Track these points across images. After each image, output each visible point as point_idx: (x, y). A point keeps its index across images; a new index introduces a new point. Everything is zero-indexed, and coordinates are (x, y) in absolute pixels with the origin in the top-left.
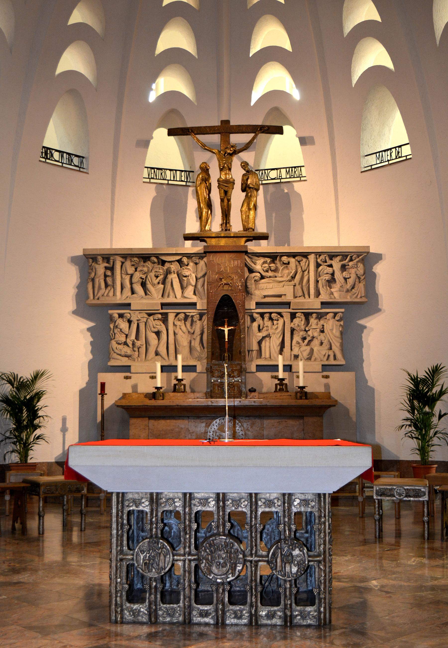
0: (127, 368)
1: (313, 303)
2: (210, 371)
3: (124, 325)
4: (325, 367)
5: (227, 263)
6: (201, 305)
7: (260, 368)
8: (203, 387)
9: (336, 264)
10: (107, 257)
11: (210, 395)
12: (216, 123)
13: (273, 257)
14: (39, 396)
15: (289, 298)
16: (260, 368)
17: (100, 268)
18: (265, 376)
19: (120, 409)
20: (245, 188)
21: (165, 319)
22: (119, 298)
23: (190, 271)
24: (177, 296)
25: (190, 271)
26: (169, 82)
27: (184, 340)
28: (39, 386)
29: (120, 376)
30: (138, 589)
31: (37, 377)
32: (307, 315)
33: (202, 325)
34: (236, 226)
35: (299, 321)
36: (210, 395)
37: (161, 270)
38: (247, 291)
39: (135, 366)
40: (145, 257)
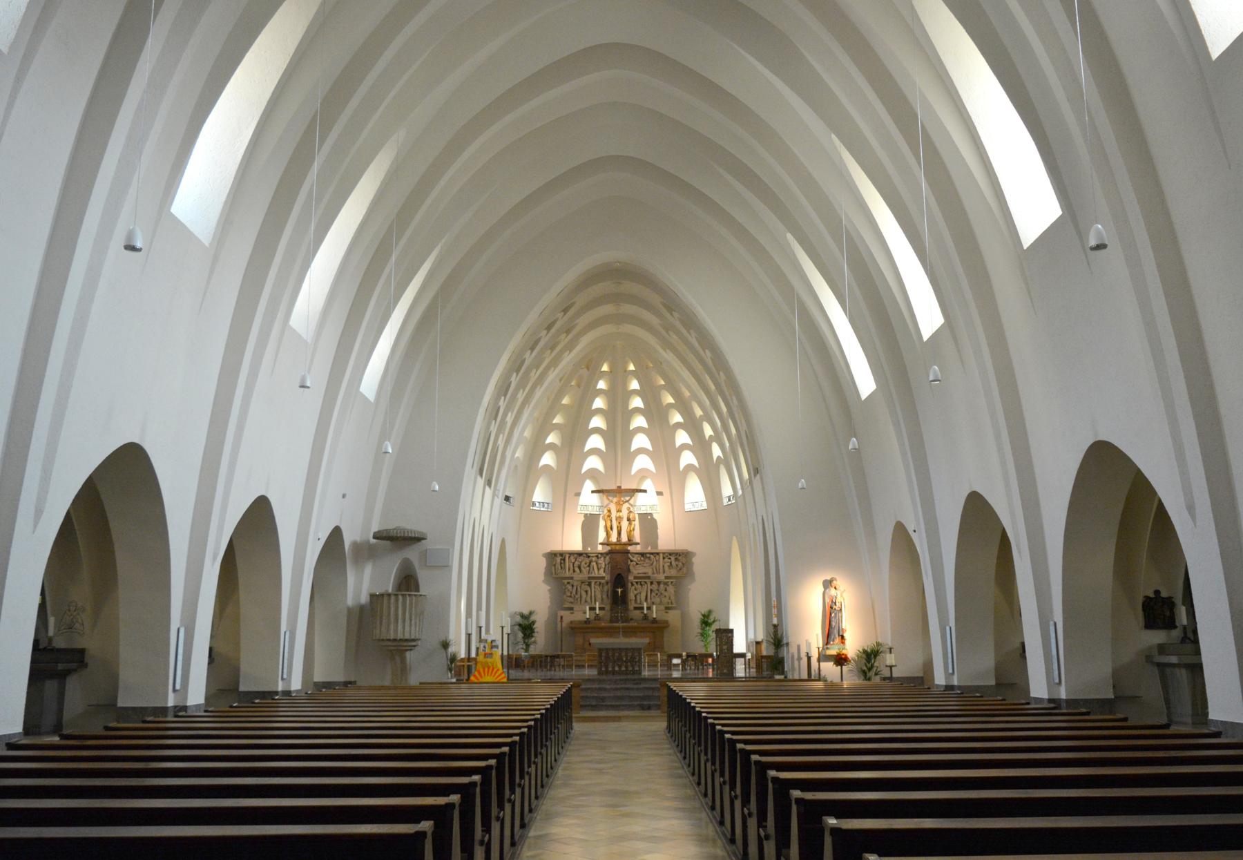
0: (572, 609)
1: (661, 577)
2: (611, 610)
3: (569, 587)
4: (667, 608)
5: (618, 557)
6: (608, 578)
7: (636, 608)
8: (608, 618)
9: (673, 558)
10: (562, 554)
11: (611, 621)
12: (614, 487)
13: (642, 554)
14: (534, 623)
15: (650, 574)
16: (636, 608)
17: (558, 559)
18: (638, 612)
19: (595, 495)
20: (629, 520)
21: (589, 585)
22: (567, 574)
23: (601, 561)
24: (596, 573)
25: (601, 561)
26: (593, 463)
27: (599, 596)
28: (533, 618)
29: (568, 612)
30: (546, 466)
31: (531, 613)
32: (659, 583)
33: (608, 588)
34: (624, 539)
35: (655, 587)
36: (611, 621)
37: (588, 561)
38: (629, 571)
39: (576, 607)
40: (580, 554)
